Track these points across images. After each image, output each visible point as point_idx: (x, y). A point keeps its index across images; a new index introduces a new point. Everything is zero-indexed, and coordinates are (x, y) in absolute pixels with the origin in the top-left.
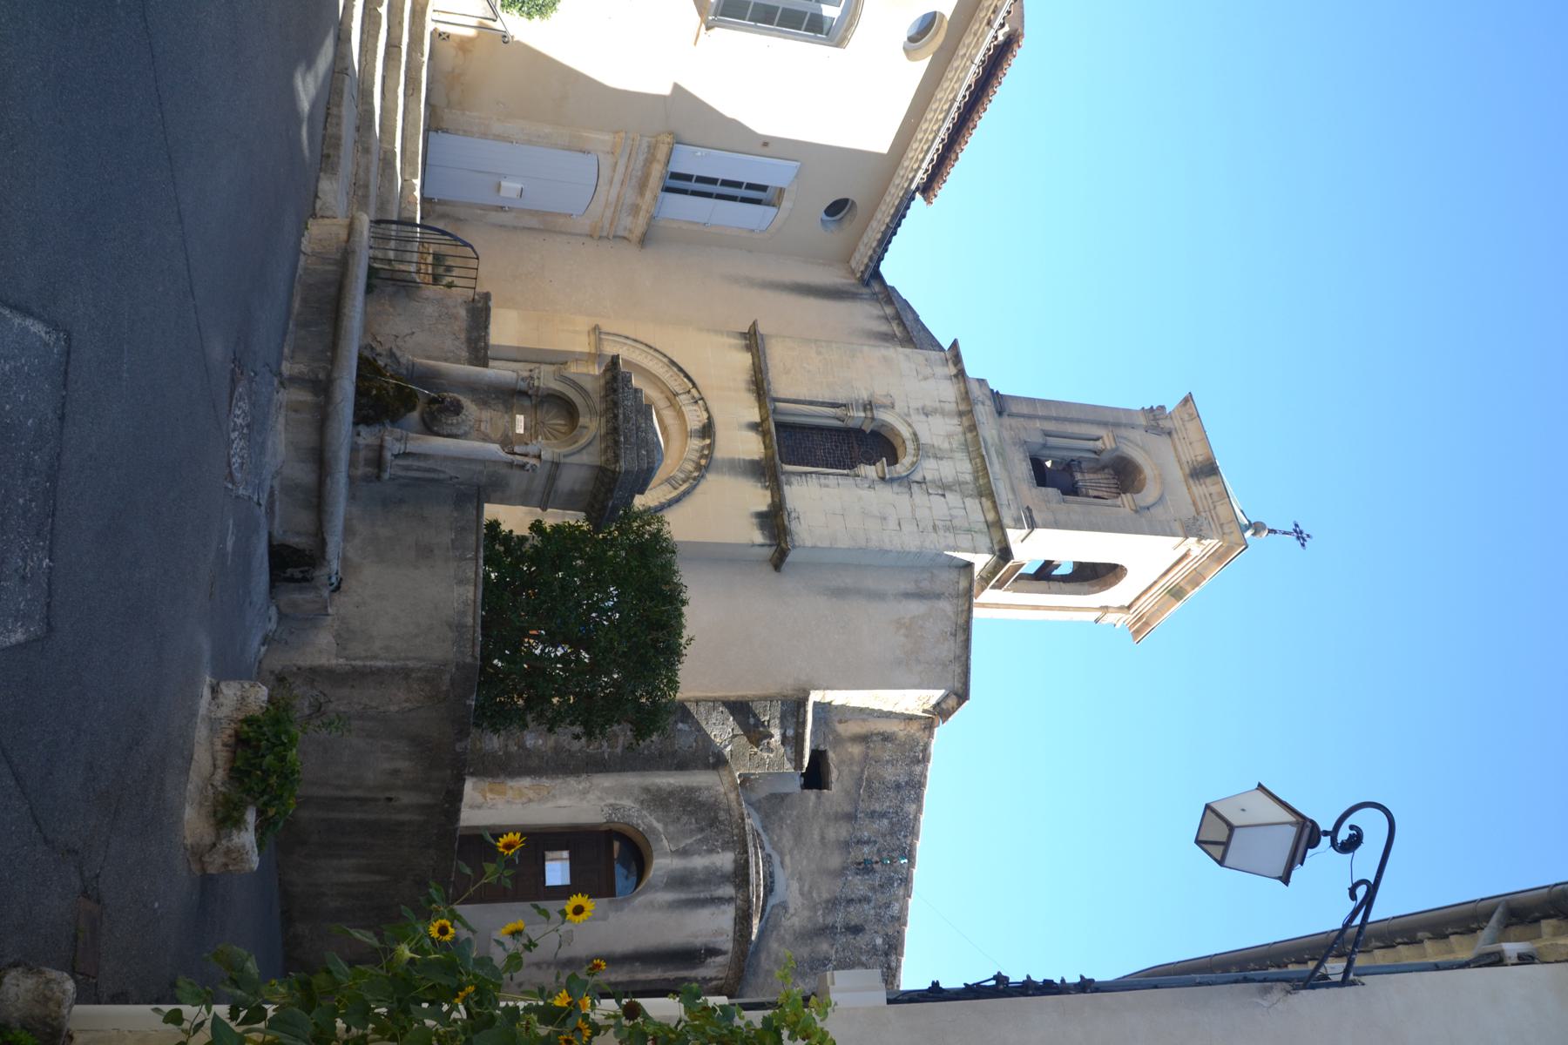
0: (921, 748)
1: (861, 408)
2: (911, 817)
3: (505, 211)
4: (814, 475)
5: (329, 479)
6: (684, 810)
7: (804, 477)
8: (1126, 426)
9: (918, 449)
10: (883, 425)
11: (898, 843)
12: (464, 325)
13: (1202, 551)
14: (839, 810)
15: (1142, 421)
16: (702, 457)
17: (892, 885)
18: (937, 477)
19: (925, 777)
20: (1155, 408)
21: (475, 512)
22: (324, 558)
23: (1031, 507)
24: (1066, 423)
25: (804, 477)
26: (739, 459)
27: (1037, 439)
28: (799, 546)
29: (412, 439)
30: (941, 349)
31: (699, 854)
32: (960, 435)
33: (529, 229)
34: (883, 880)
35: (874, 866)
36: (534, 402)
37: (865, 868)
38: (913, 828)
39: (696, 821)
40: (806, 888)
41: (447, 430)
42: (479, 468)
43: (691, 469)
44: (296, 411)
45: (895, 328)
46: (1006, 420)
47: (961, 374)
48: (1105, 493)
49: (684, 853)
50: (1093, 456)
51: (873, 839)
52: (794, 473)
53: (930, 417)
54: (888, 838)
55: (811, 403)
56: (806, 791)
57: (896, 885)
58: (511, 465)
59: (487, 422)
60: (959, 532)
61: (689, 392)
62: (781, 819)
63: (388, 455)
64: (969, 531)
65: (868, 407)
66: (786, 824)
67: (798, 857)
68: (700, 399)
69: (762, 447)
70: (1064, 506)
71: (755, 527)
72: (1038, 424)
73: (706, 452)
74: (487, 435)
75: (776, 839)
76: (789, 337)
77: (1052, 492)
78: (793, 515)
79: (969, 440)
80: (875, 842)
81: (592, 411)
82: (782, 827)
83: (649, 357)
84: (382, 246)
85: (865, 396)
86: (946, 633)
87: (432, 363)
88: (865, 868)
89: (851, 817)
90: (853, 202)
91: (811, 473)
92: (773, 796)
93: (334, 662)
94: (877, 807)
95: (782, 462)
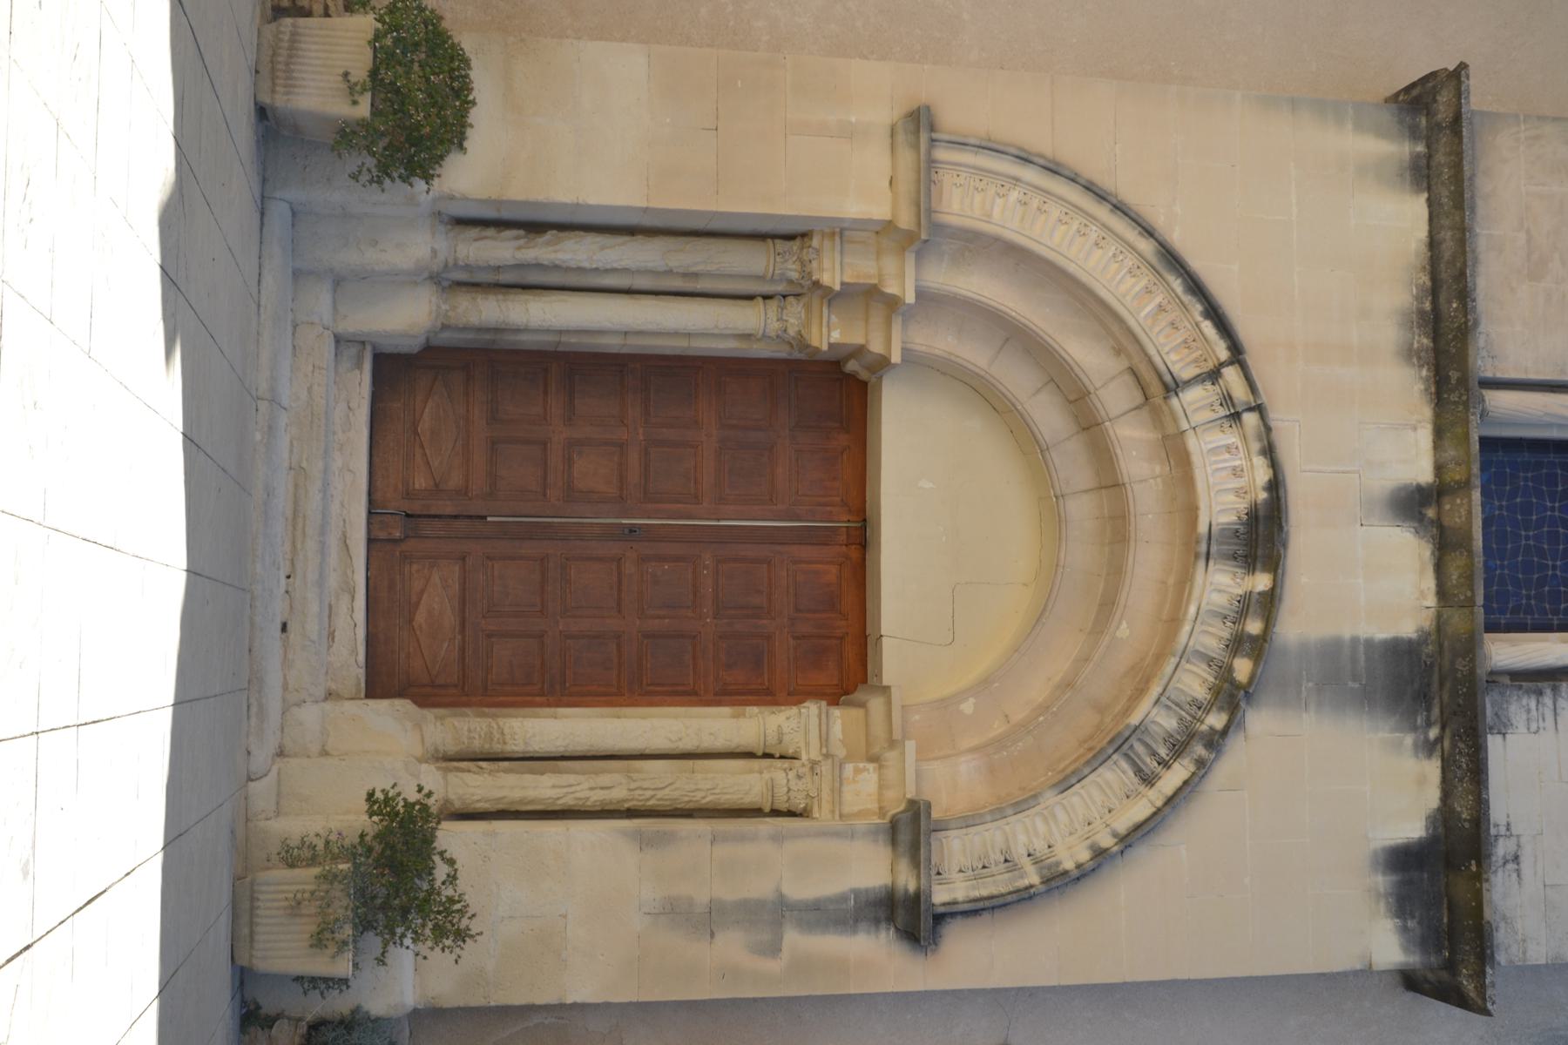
16: (1238, 643)
25: (1106, 841)
26: (1355, 641)
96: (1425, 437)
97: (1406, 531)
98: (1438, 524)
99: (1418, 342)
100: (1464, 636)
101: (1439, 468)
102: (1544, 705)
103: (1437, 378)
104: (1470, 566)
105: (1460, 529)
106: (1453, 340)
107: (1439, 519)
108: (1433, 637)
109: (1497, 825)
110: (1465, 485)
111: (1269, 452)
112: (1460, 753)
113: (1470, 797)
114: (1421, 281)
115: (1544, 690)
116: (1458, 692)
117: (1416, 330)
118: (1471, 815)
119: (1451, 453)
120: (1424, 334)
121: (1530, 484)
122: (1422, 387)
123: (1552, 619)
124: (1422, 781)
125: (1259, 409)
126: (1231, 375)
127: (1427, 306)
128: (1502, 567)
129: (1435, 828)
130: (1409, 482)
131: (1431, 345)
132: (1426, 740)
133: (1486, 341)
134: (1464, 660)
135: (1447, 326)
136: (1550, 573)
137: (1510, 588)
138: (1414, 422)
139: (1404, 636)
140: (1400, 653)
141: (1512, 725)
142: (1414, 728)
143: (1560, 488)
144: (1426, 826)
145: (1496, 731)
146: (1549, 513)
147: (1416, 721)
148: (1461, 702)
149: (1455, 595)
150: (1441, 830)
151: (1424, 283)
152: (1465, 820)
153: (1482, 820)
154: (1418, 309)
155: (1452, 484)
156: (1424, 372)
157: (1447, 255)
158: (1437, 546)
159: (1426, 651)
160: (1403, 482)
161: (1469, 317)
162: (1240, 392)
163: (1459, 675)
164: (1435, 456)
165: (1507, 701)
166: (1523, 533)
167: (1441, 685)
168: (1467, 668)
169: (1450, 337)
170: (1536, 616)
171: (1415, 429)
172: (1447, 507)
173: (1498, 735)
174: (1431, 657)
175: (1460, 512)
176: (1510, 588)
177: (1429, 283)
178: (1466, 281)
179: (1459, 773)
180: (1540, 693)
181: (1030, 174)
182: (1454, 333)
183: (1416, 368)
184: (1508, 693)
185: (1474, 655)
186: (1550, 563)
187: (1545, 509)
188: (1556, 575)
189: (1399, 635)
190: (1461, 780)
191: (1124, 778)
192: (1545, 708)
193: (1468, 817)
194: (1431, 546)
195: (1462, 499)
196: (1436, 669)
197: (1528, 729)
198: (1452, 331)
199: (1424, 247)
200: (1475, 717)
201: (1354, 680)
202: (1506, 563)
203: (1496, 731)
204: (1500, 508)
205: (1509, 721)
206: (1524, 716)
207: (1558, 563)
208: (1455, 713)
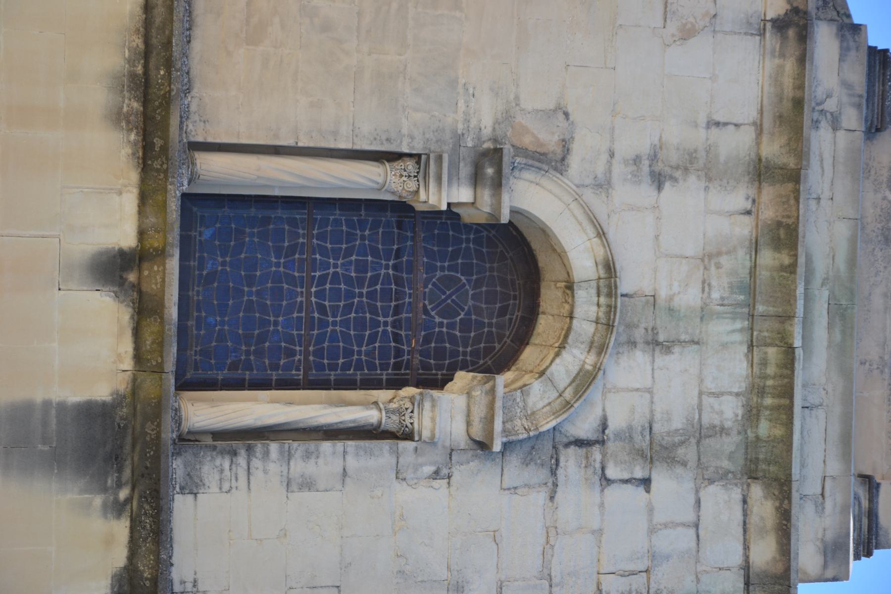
26: (47, 404)
96: (130, 201)
97: (106, 295)
98: (137, 287)
99: (128, 106)
100: (154, 401)
101: (142, 234)
102: (238, 465)
103: (144, 144)
104: (162, 333)
105: (156, 295)
106: (158, 108)
107: (139, 283)
108: (128, 400)
109: (183, 582)
110: (161, 254)
112: (145, 514)
113: (152, 557)
114: (134, 44)
115: (238, 451)
116: (146, 455)
117: (127, 94)
118: (151, 574)
119: (152, 220)
120: (135, 97)
121: (256, 240)
122: (130, 151)
123: (272, 375)
124: (109, 541)
127: (139, 69)
128: (223, 323)
129: (120, 586)
130: (110, 246)
131: (142, 109)
132: (116, 500)
133: (198, 105)
134: (152, 423)
135: (154, 93)
136: (272, 328)
137: (229, 344)
138: (120, 187)
139: (98, 399)
141: (204, 485)
142: (104, 490)
143: (286, 244)
144: (112, 584)
145: (187, 491)
146: (274, 269)
147: (106, 482)
148: (148, 465)
149: (148, 360)
150: (126, 588)
151: (138, 46)
152: (147, 579)
153: (159, 579)
154: (129, 72)
155: (151, 250)
156: (133, 137)
157: (158, 21)
158: (137, 310)
159: (121, 414)
160: (105, 246)
161: (172, 86)
163: (148, 439)
164: (139, 220)
165: (200, 462)
166: (246, 289)
167: (133, 446)
168: (155, 432)
169: (157, 103)
170: (255, 372)
171: (120, 193)
172: (146, 273)
173: (189, 495)
174: (125, 420)
175: (156, 280)
176: (229, 344)
177: (142, 46)
178: (172, 50)
179: (143, 533)
180: (234, 453)
182: (160, 101)
183: (125, 132)
184: (202, 453)
185: (160, 421)
186: (272, 319)
187: (270, 264)
188: (278, 330)
189: (93, 398)
190: (145, 540)
191: (859, 234)
192: (239, 468)
193: (149, 576)
194: (130, 310)
195: (158, 267)
196: (130, 431)
197: (221, 488)
198: (159, 98)
199: (138, 9)
200: (159, 480)
201: (44, 444)
202: (226, 319)
203: (187, 491)
204: (224, 264)
205: (201, 481)
206: (217, 477)
207: (281, 319)
208: (143, 476)
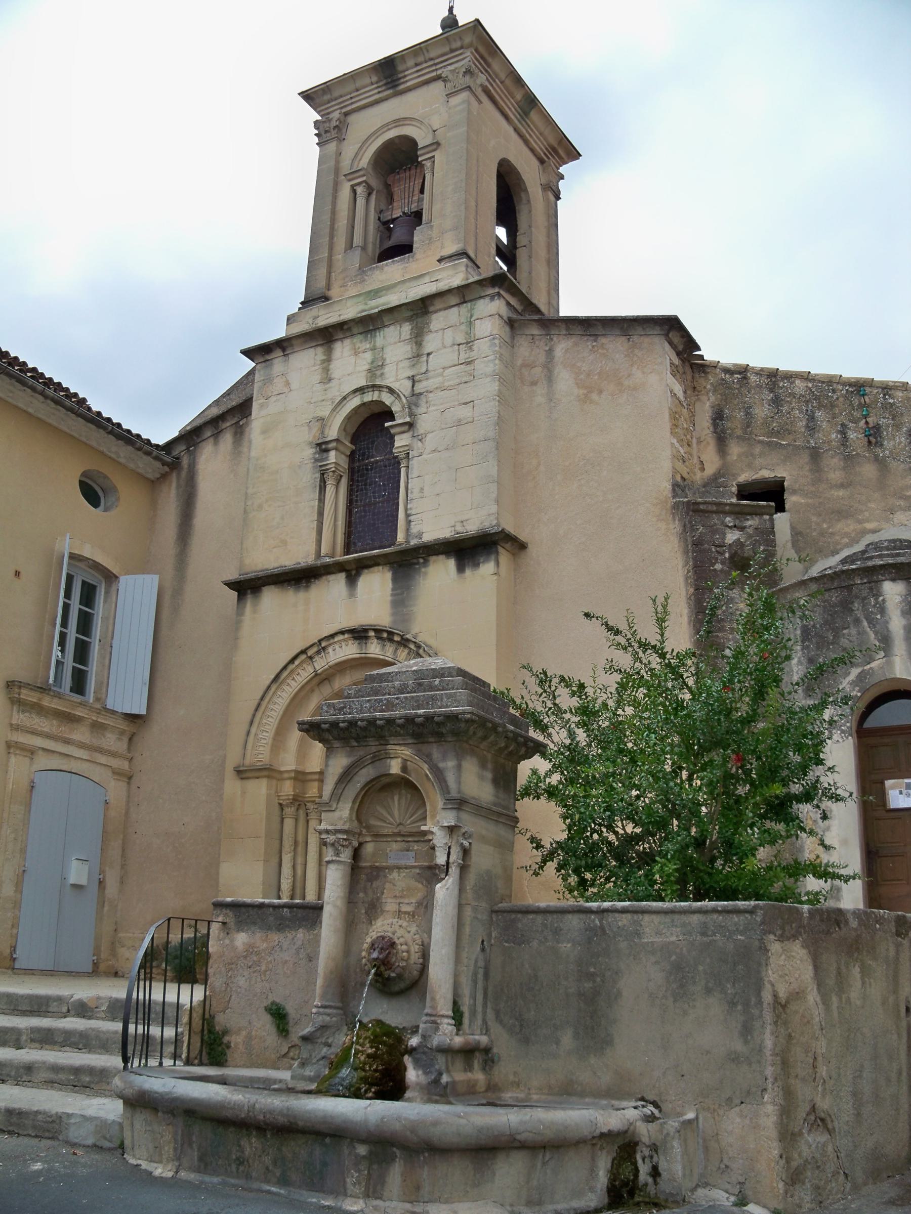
0: (728, 376)
1: (325, 455)
2: (810, 385)
3: (104, 878)
4: (409, 507)
5: (518, 1137)
6: (832, 644)
7: (411, 518)
8: (337, 162)
9: (374, 387)
10: (345, 430)
11: (841, 399)
12: (259, 935)
13: (482, 73)
14: (807, 468)
15: (332, 147)
16: (391, 640)
17: (892, 405)
18: (407, 363)
19: (762, 370)
20: (317, 132)
21: (531, 916)
22: (626, 1132)
23: (438, 258)
24: (336, 227)
25: (411, 518)
26: (392, 595)
27: (356, 257)
28: (497, 519)
29: (434, 1007)
30: (252, 373)
31: (887, 622)
32: (355, 341)
33: (123, 850)
34: (887, 415)
35: (871, 425)
36: (368, 839)
37: (874, 436)
38: (823, 382)
39: (846, 628)
40: (902, 503)
41: (415, 958)
42: (468, 912)
43: (406, 651)
44: (418, 1188)
45: (228, 424)
46: (334, 293)
47: (282, 345)
48: (416, 182)
49: (886, 641)
50: (373, 197)
51: (839, 428)
52: (408, 530)
53: (333, 376)
54: (837, 411)
55: (321, 513)
56: (787, 506)
57: (891, 401)
58: (464, 869)
59: (400, 903)
60: (472, 335)
61: (311, 658)
62: (822, 534)
63: (458, 1041)
64: (470, 324)
65: (324, 447)
66: (829, 528)
67: (867, 514)
68: (320, 644)
69: (376, 569)
70: (435, 223)
71: (475, 572)
72: (339, 257)
73: (385, 635)
74: (419, 904)
75: (846, 540)
76: (242, 543)
77: (419, 236)
78: (459, 528)
79: (361, 330)
80: (843, 425)
81: (380, 757)
82: (831, 533)
83: (275, 699)
84: (159, 1047)
85: (310, 452)
86: (593, 347)
87: (320, 982)
88: (874, 436)
89: (815, 455)
90: (84, 474)
91: (406, 510)
92: (795, 544)
93: (770, 1108)
94: (801, 424)
95: (394, 544)
111: (333, 636)
125: (320, 641)
126: (310, 653)
140: (395, 580)
162: (315, 649)
181: (253, 730)
